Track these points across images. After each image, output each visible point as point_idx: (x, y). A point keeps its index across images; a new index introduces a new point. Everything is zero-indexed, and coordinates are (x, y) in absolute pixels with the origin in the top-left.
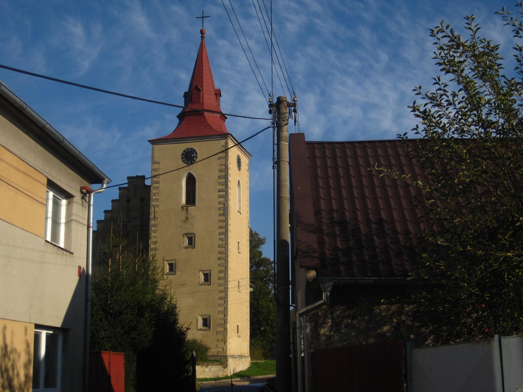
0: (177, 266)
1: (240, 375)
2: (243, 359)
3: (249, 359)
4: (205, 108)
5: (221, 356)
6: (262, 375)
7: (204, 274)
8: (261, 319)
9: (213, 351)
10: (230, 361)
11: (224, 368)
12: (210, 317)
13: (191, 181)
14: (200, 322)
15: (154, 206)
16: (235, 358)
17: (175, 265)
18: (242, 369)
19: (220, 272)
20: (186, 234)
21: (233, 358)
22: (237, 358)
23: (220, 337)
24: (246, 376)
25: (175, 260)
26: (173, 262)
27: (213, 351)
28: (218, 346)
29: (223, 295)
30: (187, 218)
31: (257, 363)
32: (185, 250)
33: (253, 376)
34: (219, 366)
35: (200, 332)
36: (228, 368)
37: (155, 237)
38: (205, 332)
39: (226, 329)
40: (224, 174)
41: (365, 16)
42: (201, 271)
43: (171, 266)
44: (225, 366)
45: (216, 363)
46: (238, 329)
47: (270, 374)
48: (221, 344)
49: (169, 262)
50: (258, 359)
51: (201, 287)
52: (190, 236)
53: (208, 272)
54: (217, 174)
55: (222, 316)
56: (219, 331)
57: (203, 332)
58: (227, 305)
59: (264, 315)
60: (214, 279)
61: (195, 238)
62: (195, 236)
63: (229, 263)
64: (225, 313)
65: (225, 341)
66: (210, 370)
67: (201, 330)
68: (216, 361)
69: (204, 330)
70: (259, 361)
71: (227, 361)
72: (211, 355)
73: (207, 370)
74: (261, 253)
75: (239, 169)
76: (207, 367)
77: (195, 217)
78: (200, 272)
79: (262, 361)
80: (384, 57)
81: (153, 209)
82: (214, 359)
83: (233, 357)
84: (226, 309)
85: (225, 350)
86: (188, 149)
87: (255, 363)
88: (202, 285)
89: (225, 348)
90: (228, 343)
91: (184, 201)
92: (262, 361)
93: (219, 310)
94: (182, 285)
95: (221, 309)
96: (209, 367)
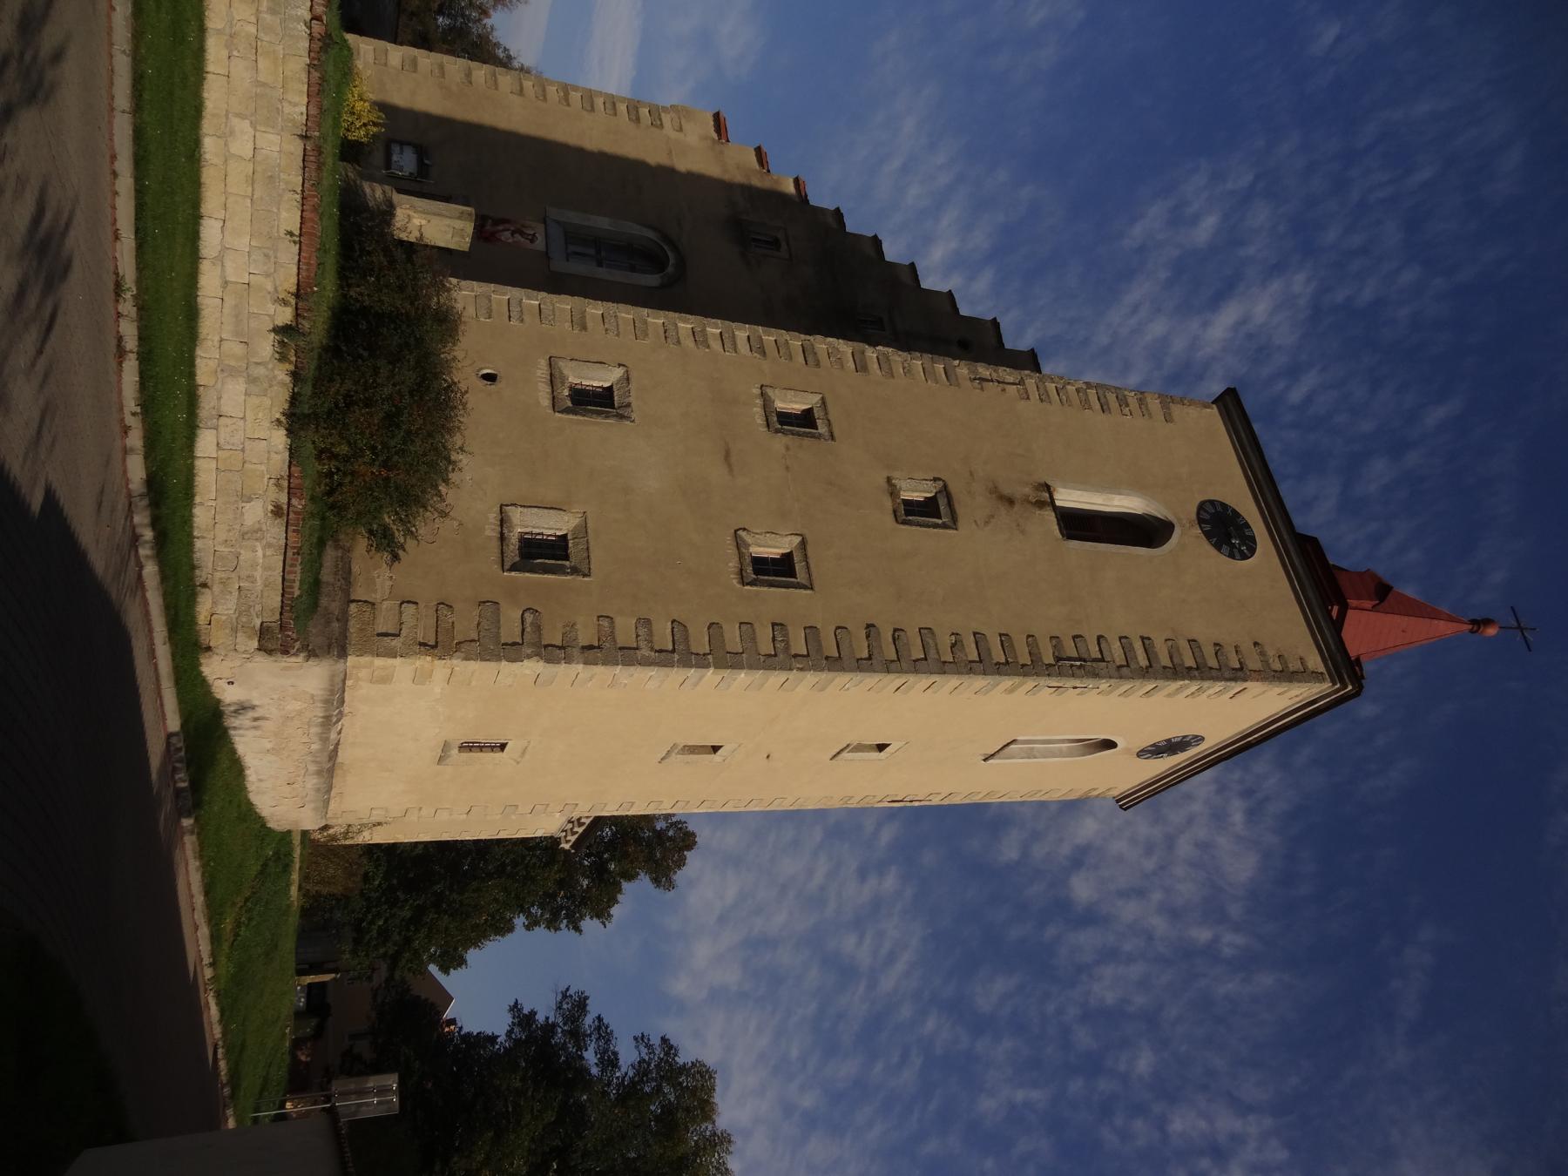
0: (807, 441)
1: (207, 731)
2: (312, 782)
3: (309, 821)
4: (1350, 613)
5: (344, 618)
6: (208, 891)
7: (788, 557)
8: (438, 888)
9: (376, 578)
10: (306, 678)
11: (264, 633)
12: (575, 571)
13: (1142, 532)
14: (550, 525)
15: (1021, 383)
16: (328, 722)
17: (813, 436)
18: (252, 776)
19: (811, 631)
20: (945, 490)
21: (327, 702)
22: (324, 740)
23: (465, 623)
24: (197, 786)
25: (832, 437)
26: (822, 429)
27: (376, 578)
28: (409, 610)
29: (700, 643)
30: (1011, 502)
31: (287, 868)
32: (882, 482)
33: (201, 830)
34: (275, 600)
35: (493, 517)
36: (263, 663)
37: (908, 371)
38: (495, 544)
39: (511, 651)
40: (1213, 663)
41: (879, 1067)
42: (803, 544)
43: (806, 420)
44: (274, 641)
45: (296, 576)
46: (481, 748)
47: (215, 938)
48: (418, 623)
49: (817, 413)
50: (305, 878)
51: (729, 539)
52: (943, 508)
53: (801, 576)
54: (1206, 634)
55: (585, 636)
56: (497, 612)
57: (491, 531)
58: (646, 663)
59: (455, 896)
60: (773, 600)
61: (936, 526)
62: (944, 526)
63: (858, 677)
64: (604, 650)
65: (438, 645)
66: (256, 533)
67: (503, 521)
68: (314, 587)
69: (502, 538)
70: (295, 876)
71: (312, 654)
72: (355, 568)
73: (256, 512)
74: (630, 877)
75: (1142, 753)
76: (277, 511)
77: (1023, 532)
78: (797, 540)
79: (294, 891)
80: (808, 1101)
81: (1011, 379)
82: (326, 575)
83: (335, 701)
84: (627, 655)
85: (383, 642)
86: (1248, 526)
87: (289, 854)
88: (739, 544)
89: (396, 643)
90: (424, 662)
91: (1068, 498)
92: (294, 891)
93: (619, 621)
94: (727, 456)
95: (625, 630)
96: (276, 532)
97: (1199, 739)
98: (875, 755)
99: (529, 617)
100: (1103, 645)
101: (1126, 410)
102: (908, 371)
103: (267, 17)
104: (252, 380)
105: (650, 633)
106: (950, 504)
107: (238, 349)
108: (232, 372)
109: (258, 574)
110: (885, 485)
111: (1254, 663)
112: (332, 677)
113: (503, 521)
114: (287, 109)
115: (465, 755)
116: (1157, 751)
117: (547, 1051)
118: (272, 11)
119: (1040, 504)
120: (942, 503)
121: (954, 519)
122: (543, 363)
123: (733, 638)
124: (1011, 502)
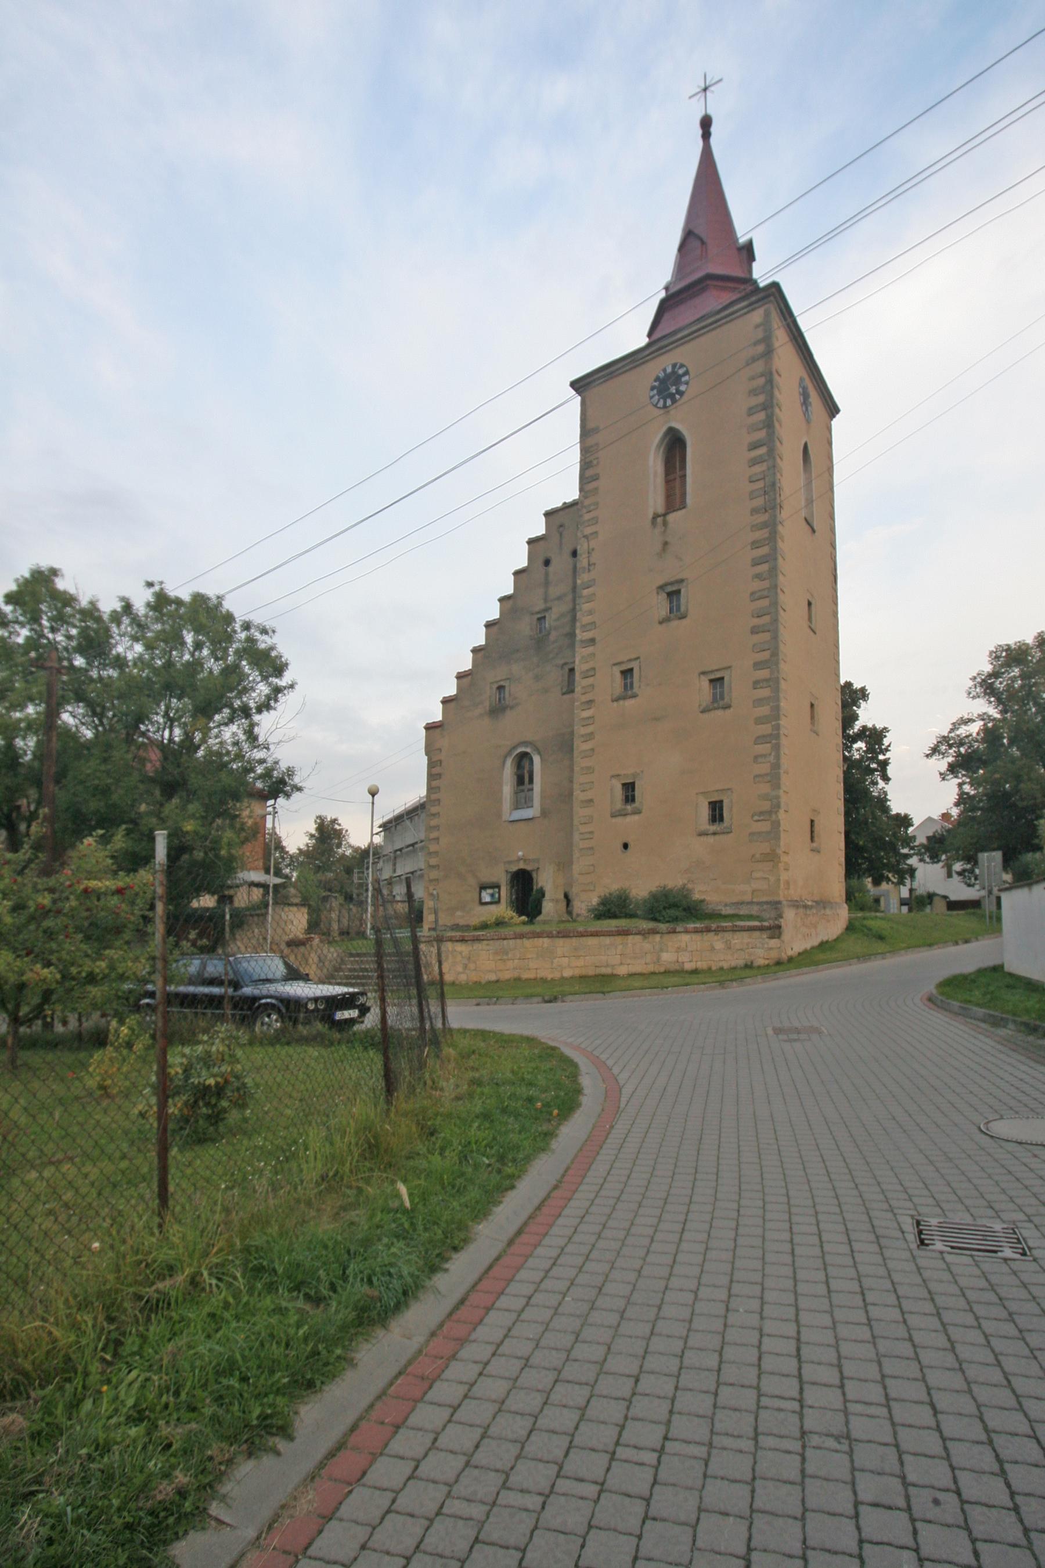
20: (661, 588)
29: (766, 729)
38: (717, 837)
57: (711, 839)
60: (738, 688)
69: (714, 834)
91: (656, 501)
97: (801, 380)
98: (813, 606)
99: (756, 818)
100: (754, 479)
101: (595, 462)
102: (590, 612)
103: (510, 956)
104: (661, 950)
105: (762, 756)
106: (671, 584)
107: (649, 956)
108: (659, 959)
109: (745, 941)
110: (664, 625)
111: (759, 366)
112: (789, 906)
113: (702, 834)
114: (545, 945)
115: (816, 839)
116: (806, 402)
117: (966, 759)
118: (507, 954)
119: (665, 524)
120: (670, 589)
121: (682, 581)
122: (614, 820)
123: (764, 710)
124: (666, 543)
